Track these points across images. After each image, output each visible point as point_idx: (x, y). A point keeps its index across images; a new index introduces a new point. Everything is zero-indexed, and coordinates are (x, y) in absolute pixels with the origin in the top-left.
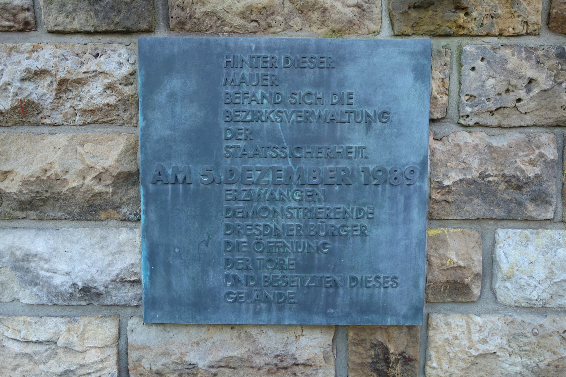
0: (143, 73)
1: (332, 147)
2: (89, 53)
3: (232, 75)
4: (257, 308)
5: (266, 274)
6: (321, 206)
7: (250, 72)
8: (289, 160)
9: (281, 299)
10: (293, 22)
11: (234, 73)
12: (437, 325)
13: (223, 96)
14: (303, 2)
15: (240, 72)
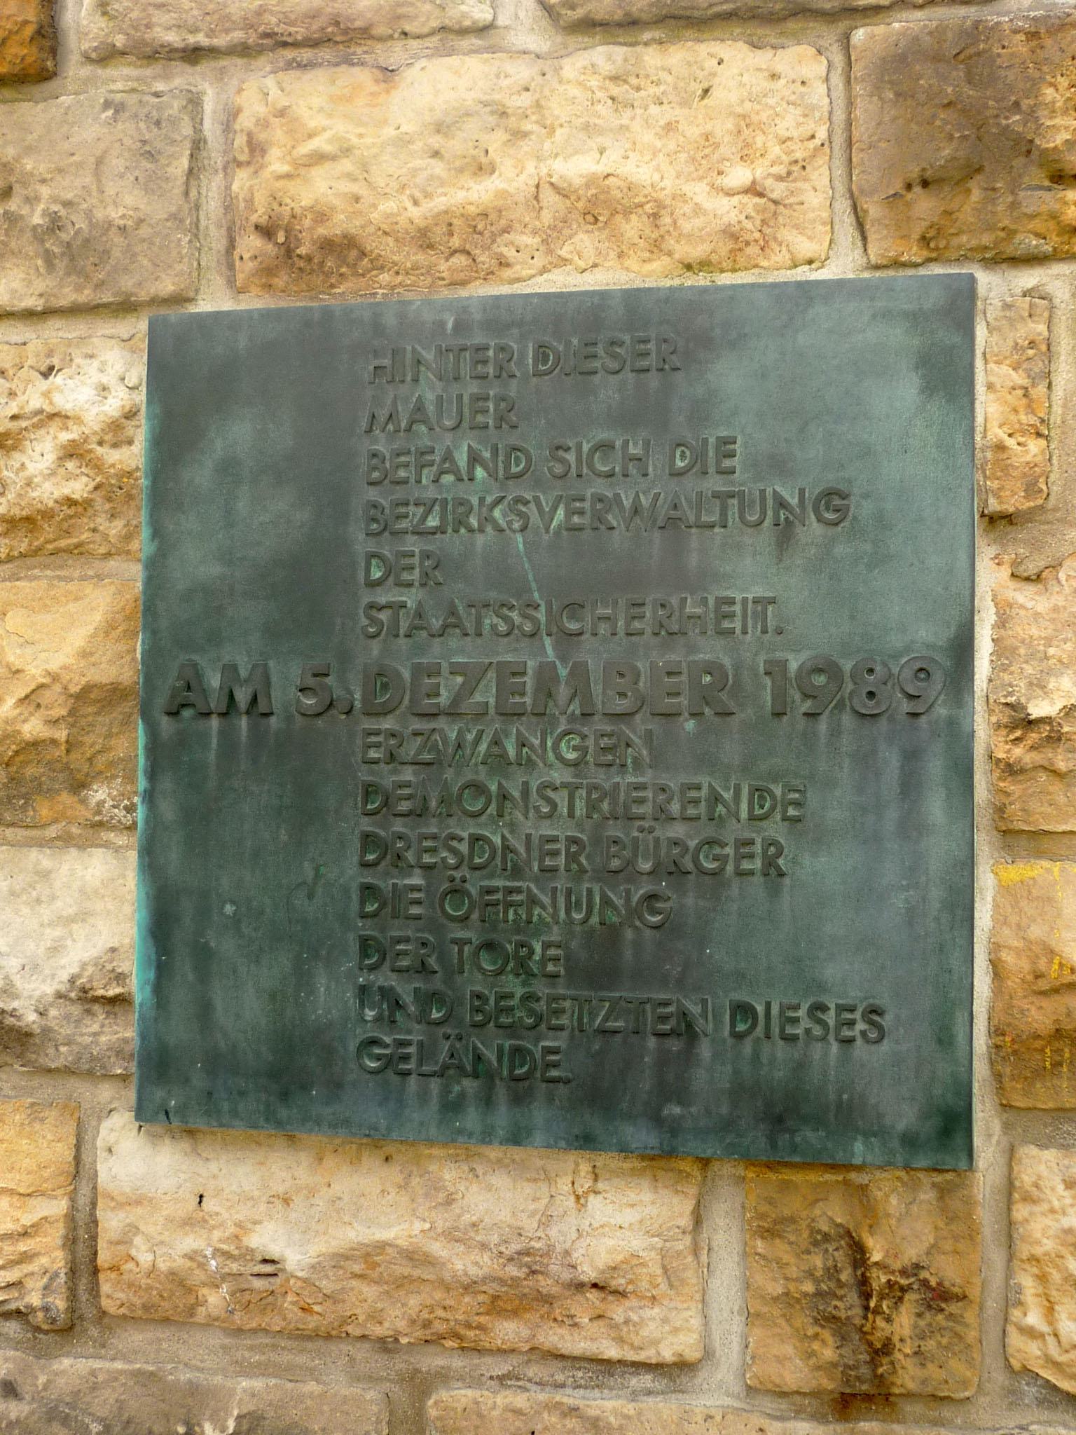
0: (158, 411)
1: (674, 601)
2: (32, 367)
3: (389, 402)
4: (450, 1092)
5: (478, 988)
6: (640, 779)
7: (439, 392)
8: (548, 641)
9: (522, 1066)
10: (572, 248)
11: (395, 397)
12: (1037, 1186)
13: (363, 462)
14: (594, 191)
15: (412, 394)
